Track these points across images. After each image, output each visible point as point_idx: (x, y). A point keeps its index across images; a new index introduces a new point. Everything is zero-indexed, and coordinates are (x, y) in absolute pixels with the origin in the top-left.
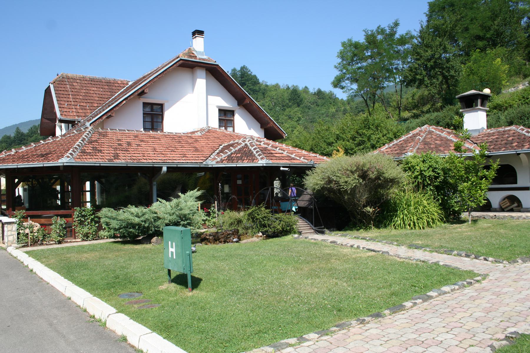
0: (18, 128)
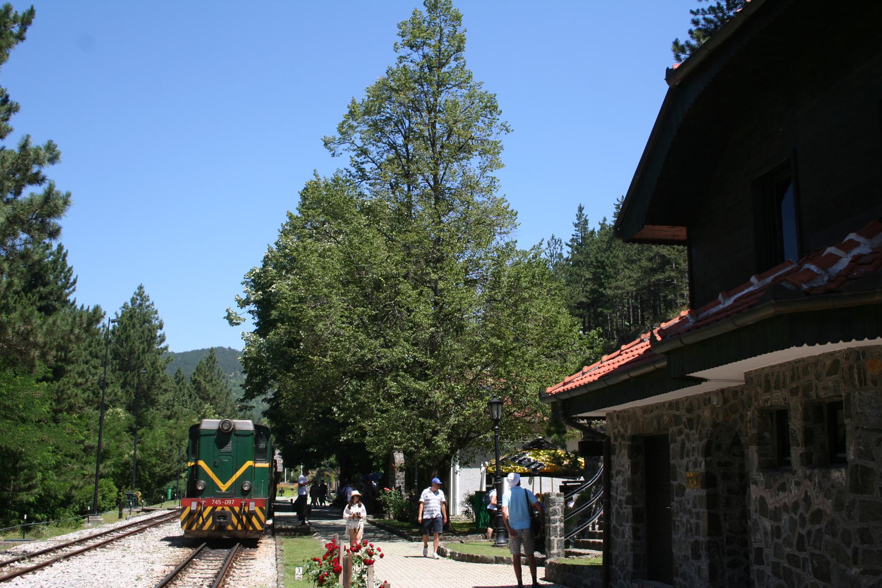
0: (141, 288)
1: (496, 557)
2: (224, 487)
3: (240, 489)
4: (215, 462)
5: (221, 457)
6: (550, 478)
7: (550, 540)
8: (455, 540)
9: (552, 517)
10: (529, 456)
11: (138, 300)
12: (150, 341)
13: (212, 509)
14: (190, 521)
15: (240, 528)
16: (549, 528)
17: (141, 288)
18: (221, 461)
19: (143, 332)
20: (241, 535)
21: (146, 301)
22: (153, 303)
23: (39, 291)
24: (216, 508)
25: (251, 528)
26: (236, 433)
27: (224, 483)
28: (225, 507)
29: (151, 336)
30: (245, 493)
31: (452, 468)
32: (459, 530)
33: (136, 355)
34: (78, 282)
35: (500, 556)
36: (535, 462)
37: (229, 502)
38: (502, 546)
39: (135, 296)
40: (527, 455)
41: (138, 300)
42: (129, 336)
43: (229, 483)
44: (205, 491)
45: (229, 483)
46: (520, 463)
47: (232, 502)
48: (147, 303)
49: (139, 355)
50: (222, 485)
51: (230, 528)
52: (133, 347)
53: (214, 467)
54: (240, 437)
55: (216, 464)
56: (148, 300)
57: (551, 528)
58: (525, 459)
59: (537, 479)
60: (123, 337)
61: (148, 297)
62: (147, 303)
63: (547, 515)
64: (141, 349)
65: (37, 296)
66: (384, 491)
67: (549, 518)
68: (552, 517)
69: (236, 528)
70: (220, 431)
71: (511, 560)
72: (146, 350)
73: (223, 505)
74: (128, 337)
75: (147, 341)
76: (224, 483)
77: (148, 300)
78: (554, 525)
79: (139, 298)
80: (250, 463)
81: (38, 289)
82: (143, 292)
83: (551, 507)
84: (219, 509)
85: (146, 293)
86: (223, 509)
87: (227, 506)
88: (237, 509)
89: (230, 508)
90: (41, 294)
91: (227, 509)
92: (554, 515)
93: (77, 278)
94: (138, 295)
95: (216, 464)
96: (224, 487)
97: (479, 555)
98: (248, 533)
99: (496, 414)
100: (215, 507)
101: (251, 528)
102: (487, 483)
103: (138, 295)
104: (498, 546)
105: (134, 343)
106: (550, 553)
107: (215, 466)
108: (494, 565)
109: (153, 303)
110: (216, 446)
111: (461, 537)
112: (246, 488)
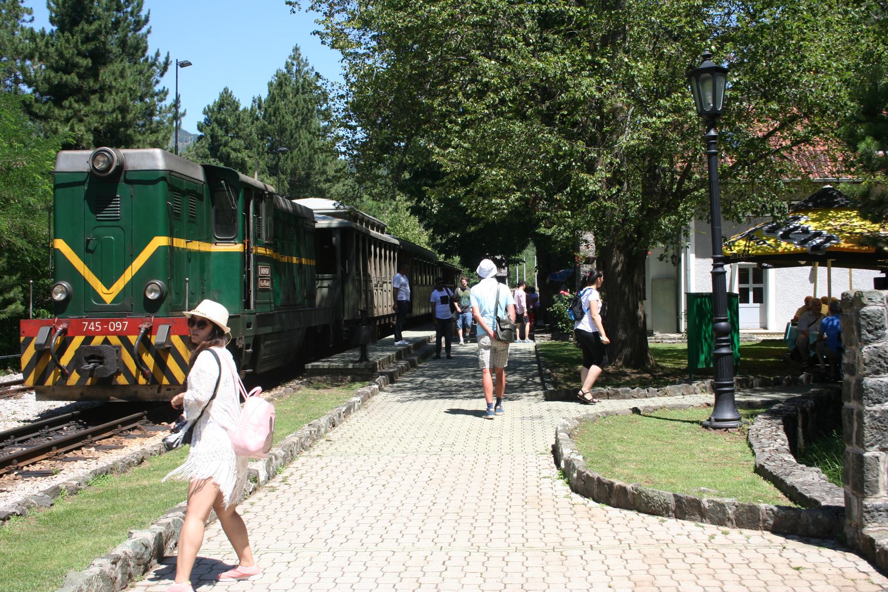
0: (296, 49)
1: (678, 499)
2: (108, 295)
3: (142, 297)
4: (88, 241)
5: (99, 231)
6: (848, 270)
7: (860, 459)
8: (639, 397)
9: (869, 381)
10: (808, 222)
11: (293, 65)
12: (306, 115)
13: (83, 343)
14: (42, 366)
15: (142, 381)
16: (860, 415)
17: (296, 49)
18: (98, 238)
19: (296, 103)
20: (149, 394)
21: (303, 66)
22: (313, 68)
23: (82, 31)
24: (92, 338)
25: (165, 381)
26: (128, 177)
27: (108, 286)
28: (110, 338)
29: (307, 108)
30: (151, 307)
31: (683, 255)
32: (669, 365)
33: (288, 133)
34: (151, 19)
35: (691, 496)
36: (818, 234)
37: (117, 325)
38: (727, 428)
39: (290, 61)
40: (802, 221)
41: (293, 65)
42: (278, 108)
43: (119, 285)
44: (70, 304)
45: (119, 285)
46: (785, 237)
47: (123, 325)
48: (306, 69)
49: (291, 132)
50: (105, 290)
51: (122, 380)
52: (282, 122)
53: (86, 252)
54: (136, 186)
55: (91, 247)
56: (307, 65)
57: (866, 420)
58: (796, 228)
59: (822, 271)
60: (271, 110)
61: (306, 60)
62: (306, 69)
63: (852, 369)
64: (294, 125)
65: (78, 37)
66: (560, 297)
67: (860, 382)
68: (869, 381)
69: (134, 381)
70: (93, 176)
71: (724, 512)
72: (299, 125)
73: (105, 332)
74: (277, 109)
75: (302, 114)
76: (108, 286)
77: (307, 65)
78: (877, 407)
79: (295, 63)
80: (161, 241)
81: (80, 27)
82: (300, 55)
83: (867, 342)
84: (98, 340)
85: (303, 56)
86: (106, 341)
87: (113, 334)
88: (134, 339)
89: (120, 338)
90: (88, 34)
91: (115, 340)
92: (877, 373)
93: (149, 13)
94: (294, 58)
95: (91, 247)
96: (108, 295)
97: (629, 487)
98: (163, 391)
99: (710, 101)
100: (89, 339)
101: (165, 381)
102: (740, 282)
103: (294, 58)
104: (715, 428)
105: (283, 117)
106: (862, 506)
107: (88, 251)
108: (672, 524)
109: (313, 68)
110: (87, 207)
111: (651, 389)
112: (152, 296)
